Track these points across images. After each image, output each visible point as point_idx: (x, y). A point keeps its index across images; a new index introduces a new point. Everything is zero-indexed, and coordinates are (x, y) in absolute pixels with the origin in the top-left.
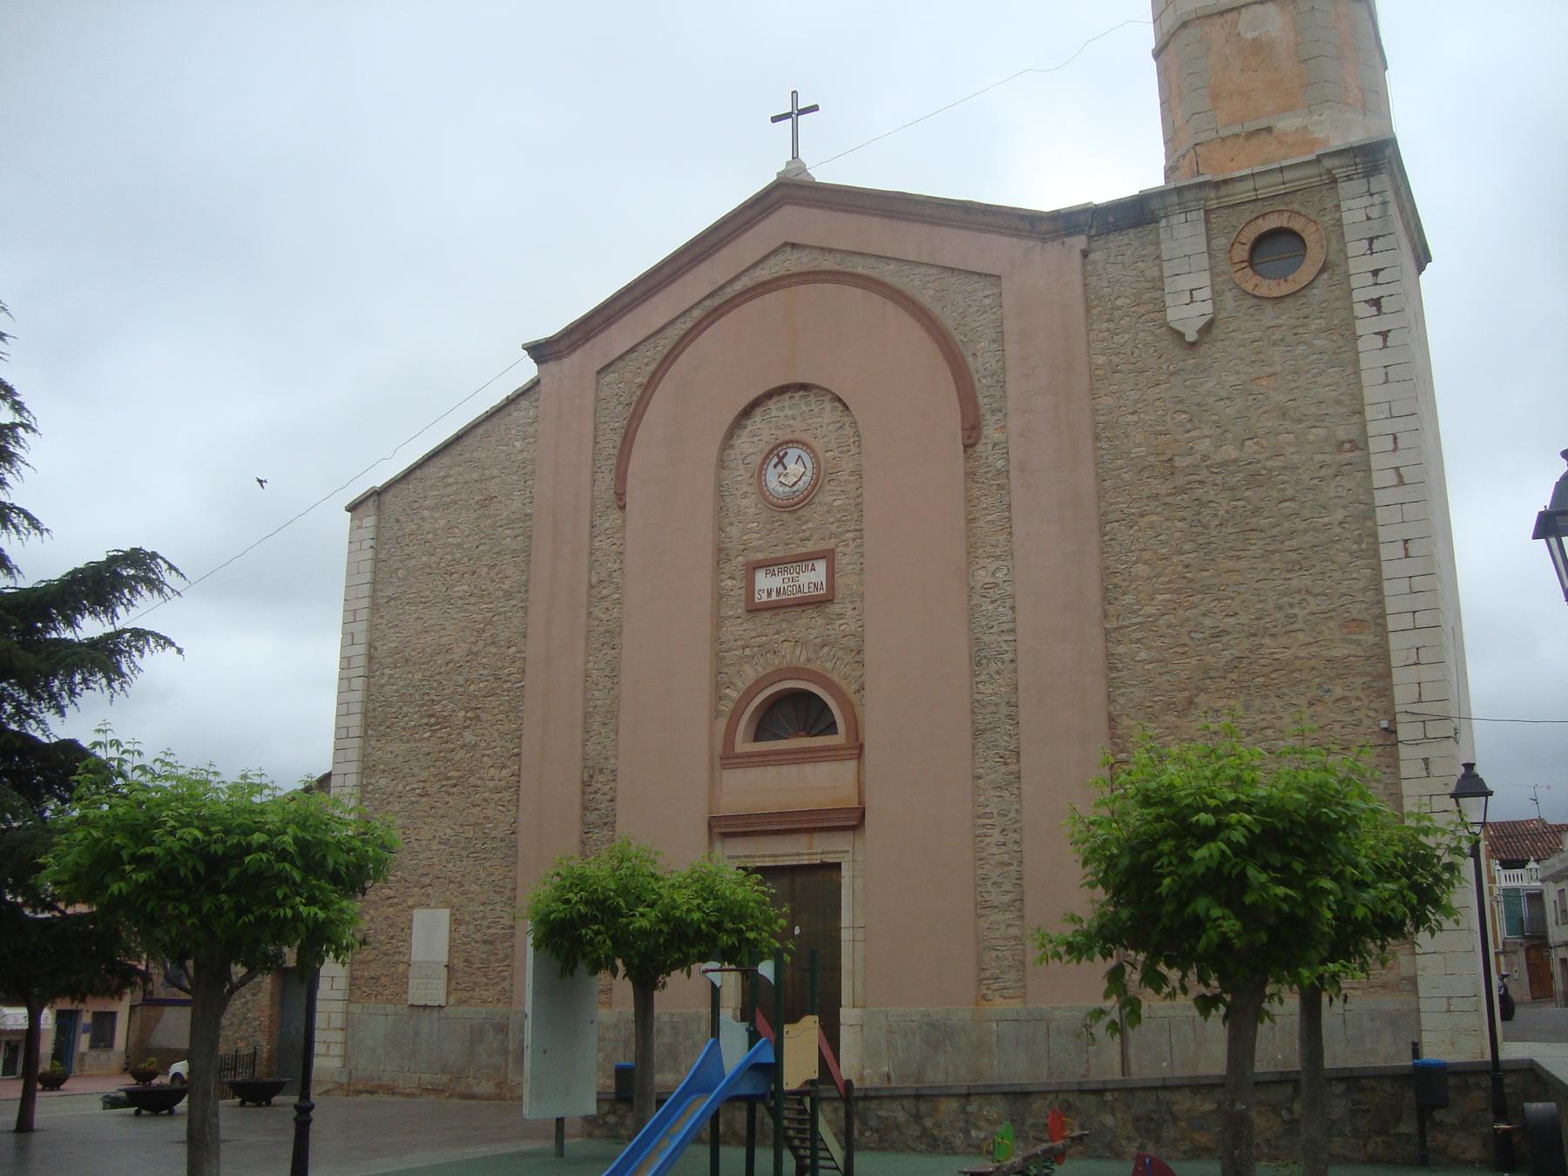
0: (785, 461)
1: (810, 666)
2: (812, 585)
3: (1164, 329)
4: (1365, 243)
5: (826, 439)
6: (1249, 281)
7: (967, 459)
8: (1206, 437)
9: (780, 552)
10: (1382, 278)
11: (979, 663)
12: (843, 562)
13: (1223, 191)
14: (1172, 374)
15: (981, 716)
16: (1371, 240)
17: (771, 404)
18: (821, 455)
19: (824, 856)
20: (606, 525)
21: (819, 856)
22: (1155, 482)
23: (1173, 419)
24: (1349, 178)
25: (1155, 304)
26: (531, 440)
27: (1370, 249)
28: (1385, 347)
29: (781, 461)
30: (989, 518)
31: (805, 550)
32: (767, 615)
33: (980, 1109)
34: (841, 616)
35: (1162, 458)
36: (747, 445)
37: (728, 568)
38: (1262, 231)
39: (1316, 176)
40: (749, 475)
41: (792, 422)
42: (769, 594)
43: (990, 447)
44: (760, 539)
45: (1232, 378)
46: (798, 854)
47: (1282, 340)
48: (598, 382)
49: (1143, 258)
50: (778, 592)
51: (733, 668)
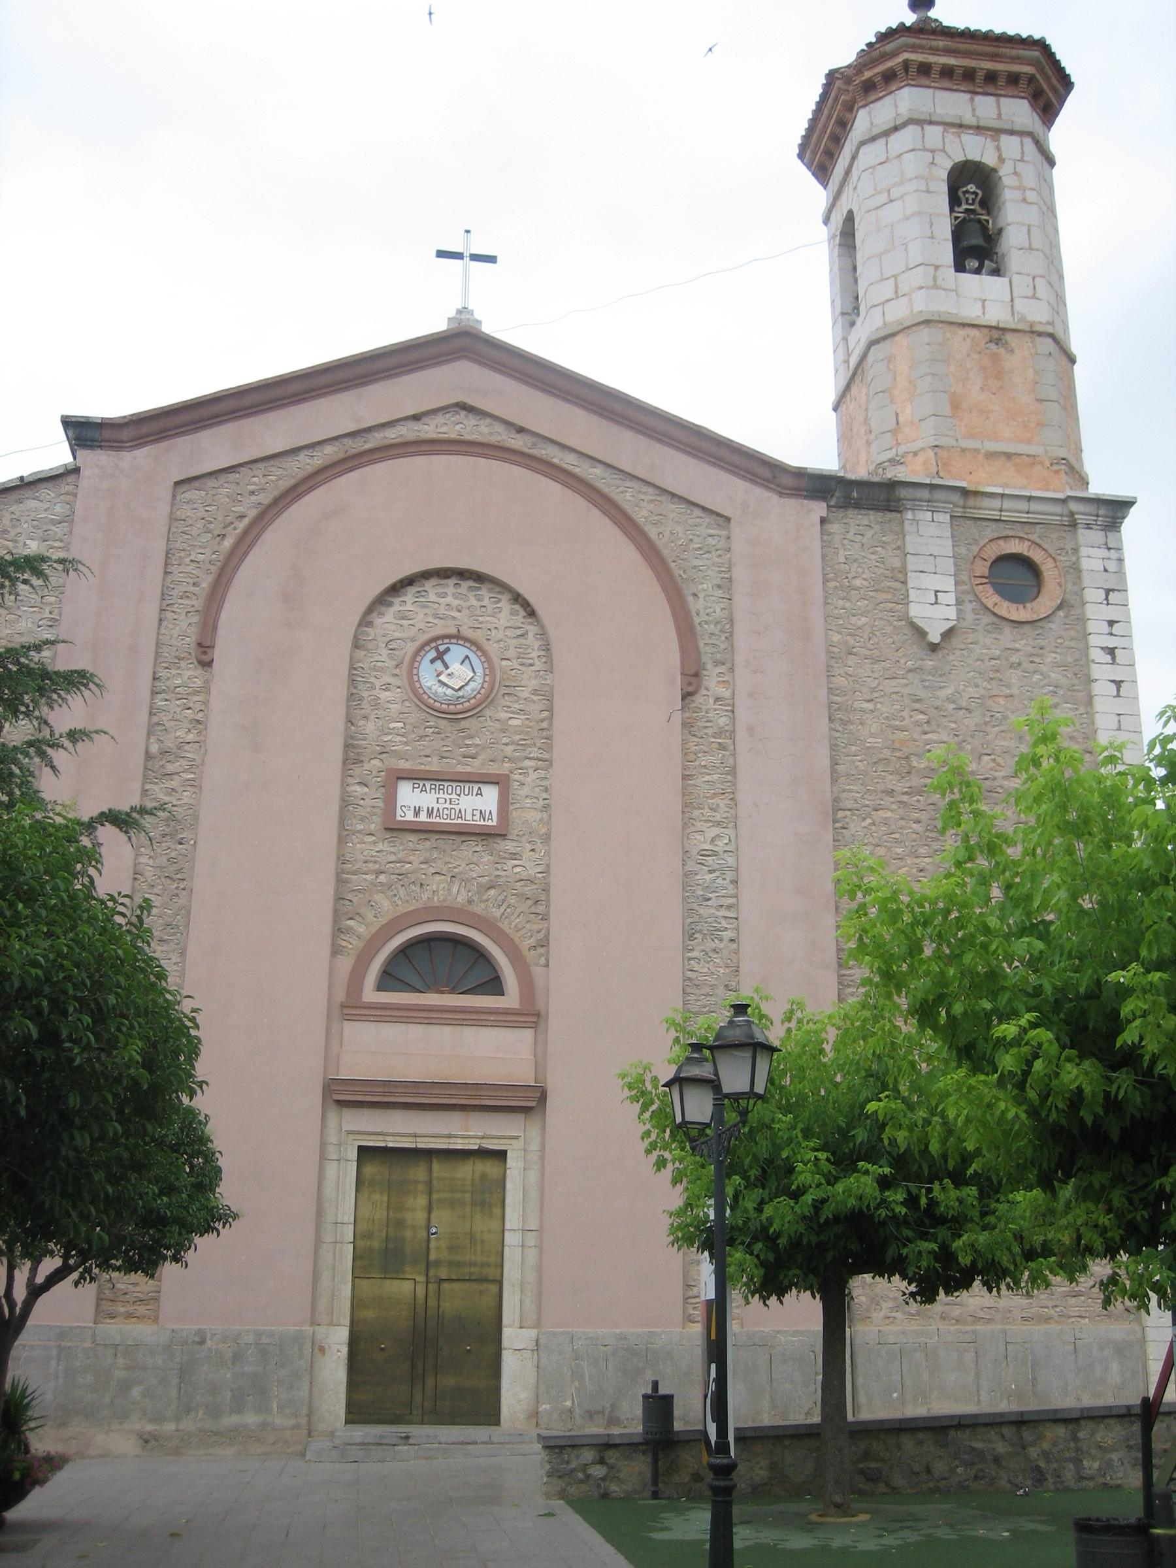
0: (446, 657)
1: (470, 908)
2: (477, 813)
3: (904, 622)
4: (1102, 593)
5: (502, 645)
6: (991, 598)
7: (683, 709)
8: (944, 742)
9: (434, 765)
10: (1116, 629)
11: (691, 937)
12: (520, 792)
13: (971, 502)
14: (910, 671)
15: (693, 997)
16: (1108, 591)
17: (429, 585)
18: (496, 661)
19: (484, 1141)
20: (179, 682)
21: (478, 1141)
22: (890, 777)
23: (911, 717)
24: (1088, 527)
25: (894, 595)
26: (57, 544)
27: (1107, 599)
28: (1118, 696)
29: (440, 656)
30: (707, 778)
31: (469, 769)
32: (413, 838)
33: (1092, 1434)
34: (514, 856)
35: (898, 754)
36: (393, 627)
37: (357, 771)
38: (1003, 553)
39: (1057, 515)
40: (395, 663)
41: (457, 614)
42: (417, 812)
43: (711, 701)
44: (406, 744)
45: (970, 689)
46: (450, 1136)
47: (1019, 664)
48: (174, 496)
49: (884, 545)
50: (430, 813)
51: (361, 896)
